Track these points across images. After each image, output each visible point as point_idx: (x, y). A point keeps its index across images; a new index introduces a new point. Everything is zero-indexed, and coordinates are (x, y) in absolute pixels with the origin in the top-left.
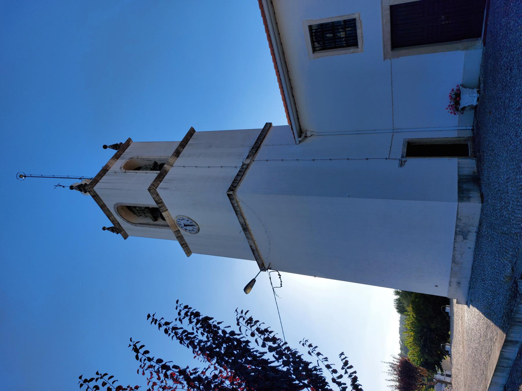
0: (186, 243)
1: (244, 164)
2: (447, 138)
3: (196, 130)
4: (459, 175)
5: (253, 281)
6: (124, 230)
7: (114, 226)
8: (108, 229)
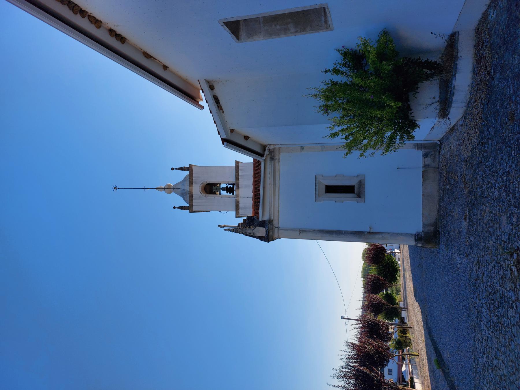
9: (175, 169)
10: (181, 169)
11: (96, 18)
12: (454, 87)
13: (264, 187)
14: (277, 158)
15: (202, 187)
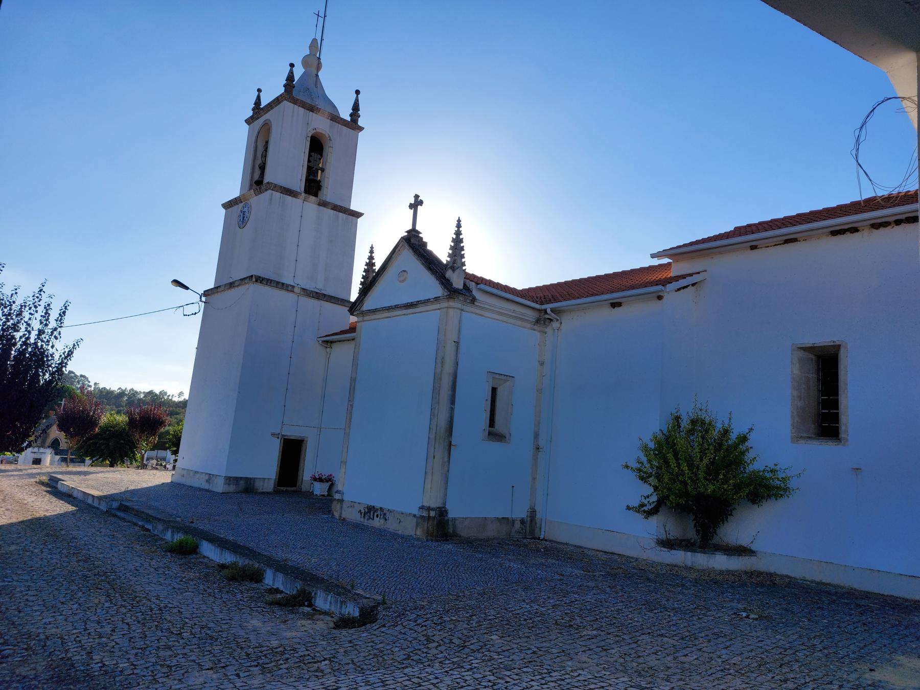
0: (232, 206)
1: (293, 287)
2: (303, 471)
3: (359, 220)
4: (254, 478)
5: (187, 288)
6: (253, 122)
7: (261, 107)
8: (259, 98)
9: (357, 96)
10: (356, 108)
11: (884, 228)
12: (715, 554)
13: (508, 300)
14: (535, 327)
15: (321, 133)
